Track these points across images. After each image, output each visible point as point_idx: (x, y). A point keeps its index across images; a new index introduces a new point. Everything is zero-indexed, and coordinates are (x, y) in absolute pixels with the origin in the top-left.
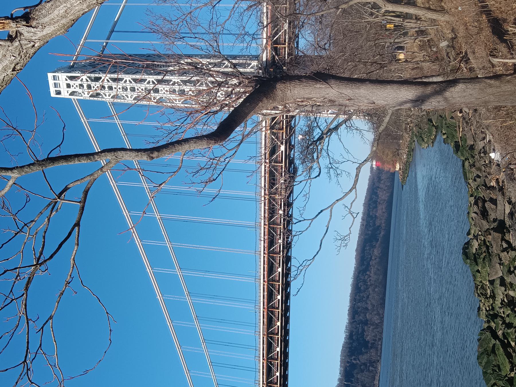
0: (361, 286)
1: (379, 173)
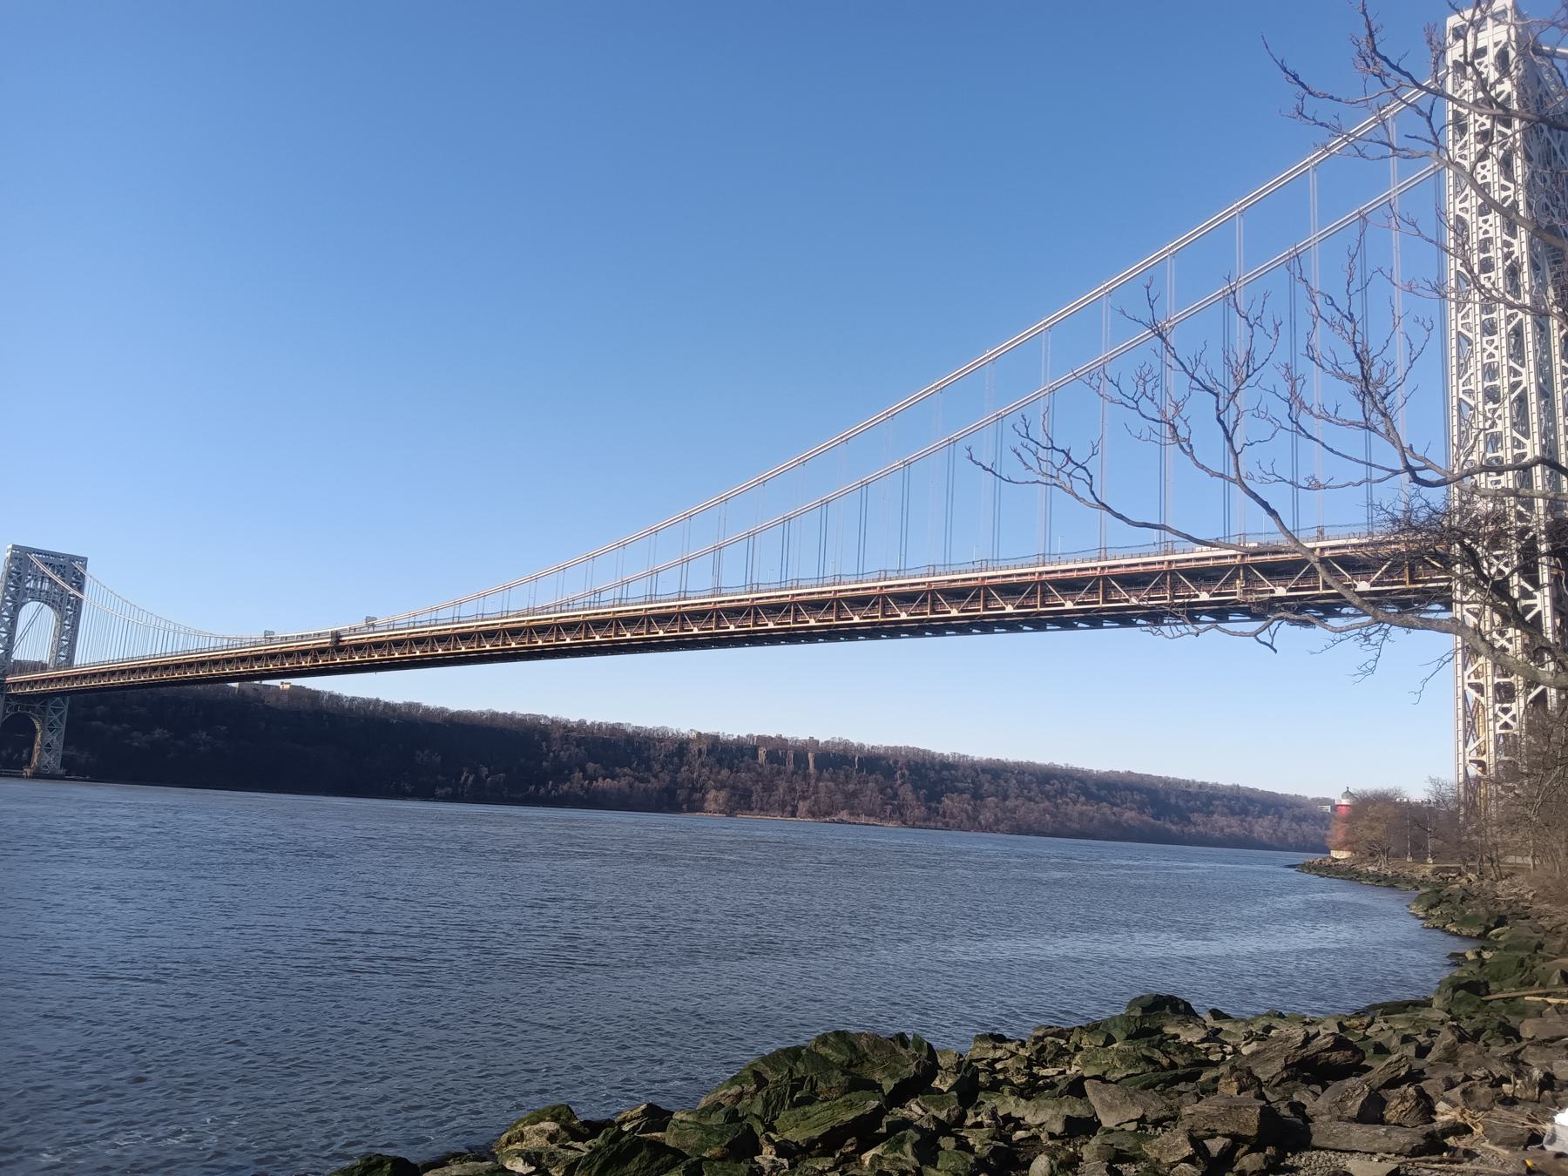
0: (1053, 785)
1: (1314, 818)
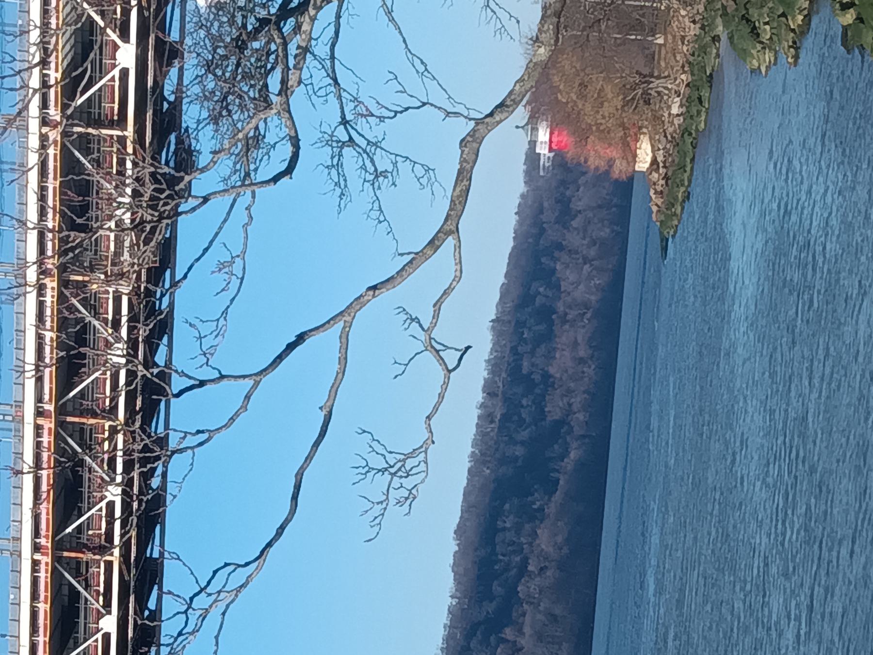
1: (563, 183)
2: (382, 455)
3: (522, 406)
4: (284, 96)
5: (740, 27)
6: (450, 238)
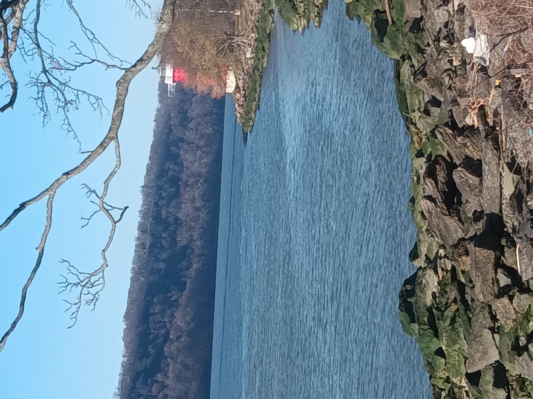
1: (183, 101)
2: (76, 275)
3: (163, 238)
4: (6, 58)
5: (286, 5)
6: (113, 141)
